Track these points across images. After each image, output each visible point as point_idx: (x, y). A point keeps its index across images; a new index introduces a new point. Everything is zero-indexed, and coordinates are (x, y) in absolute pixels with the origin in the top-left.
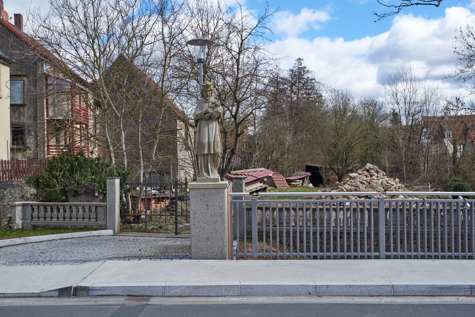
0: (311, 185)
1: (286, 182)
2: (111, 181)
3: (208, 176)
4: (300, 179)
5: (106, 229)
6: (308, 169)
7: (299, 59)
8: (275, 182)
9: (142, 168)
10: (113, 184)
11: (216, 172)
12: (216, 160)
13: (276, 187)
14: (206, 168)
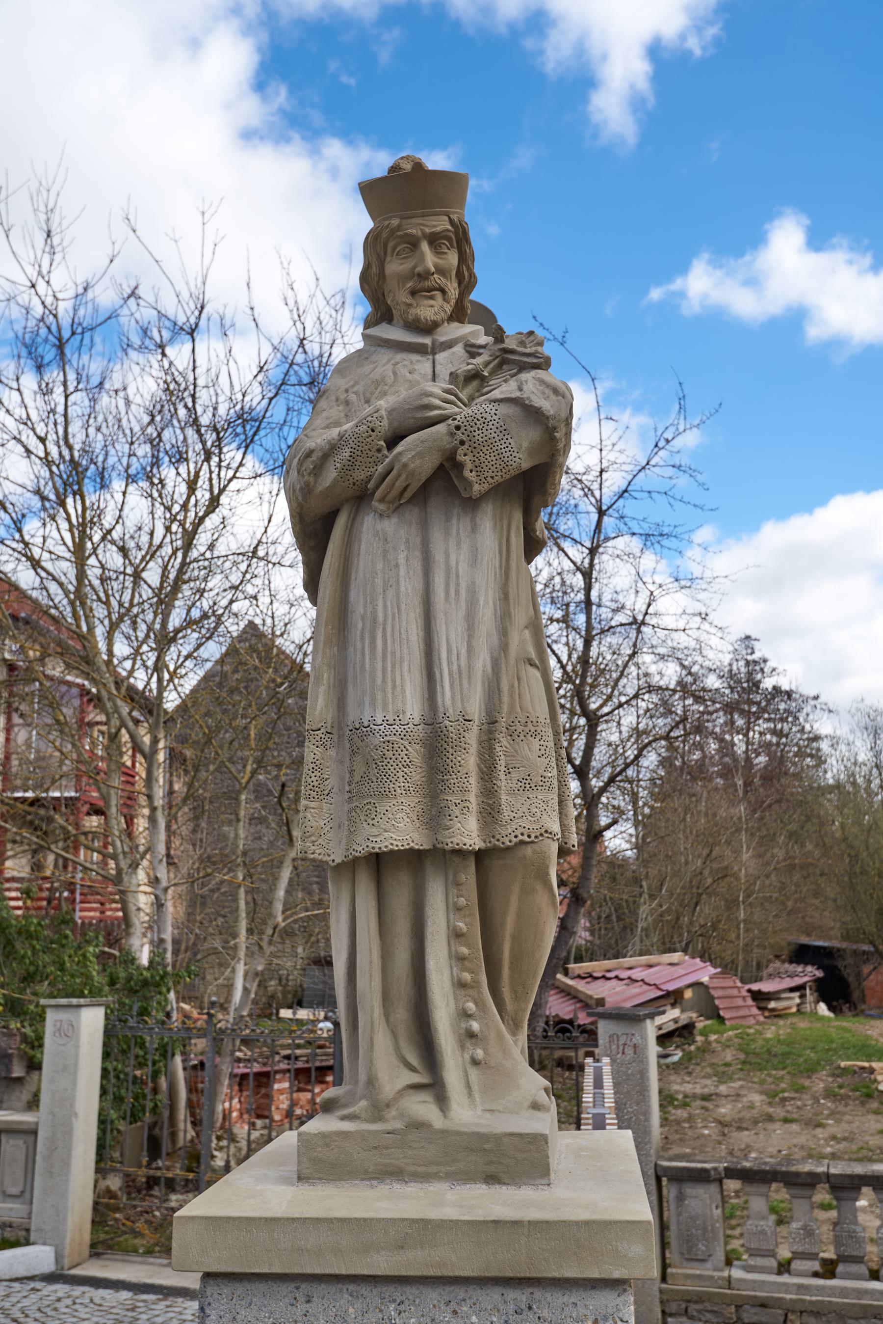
0: (823, 1009)
1: (750, 1002)
2: (63, 1015)
3: (422, 1107)
4: (792, 990)
5: (27, 1243)
6: (802, 954)
7: (748, 638)
8: (717, 1002)
9: (242, 954)
10: (70, 1033)
11: (517, 1047)
12: (509, 925)
13: (721, 1020)
14: (402, 1014)
